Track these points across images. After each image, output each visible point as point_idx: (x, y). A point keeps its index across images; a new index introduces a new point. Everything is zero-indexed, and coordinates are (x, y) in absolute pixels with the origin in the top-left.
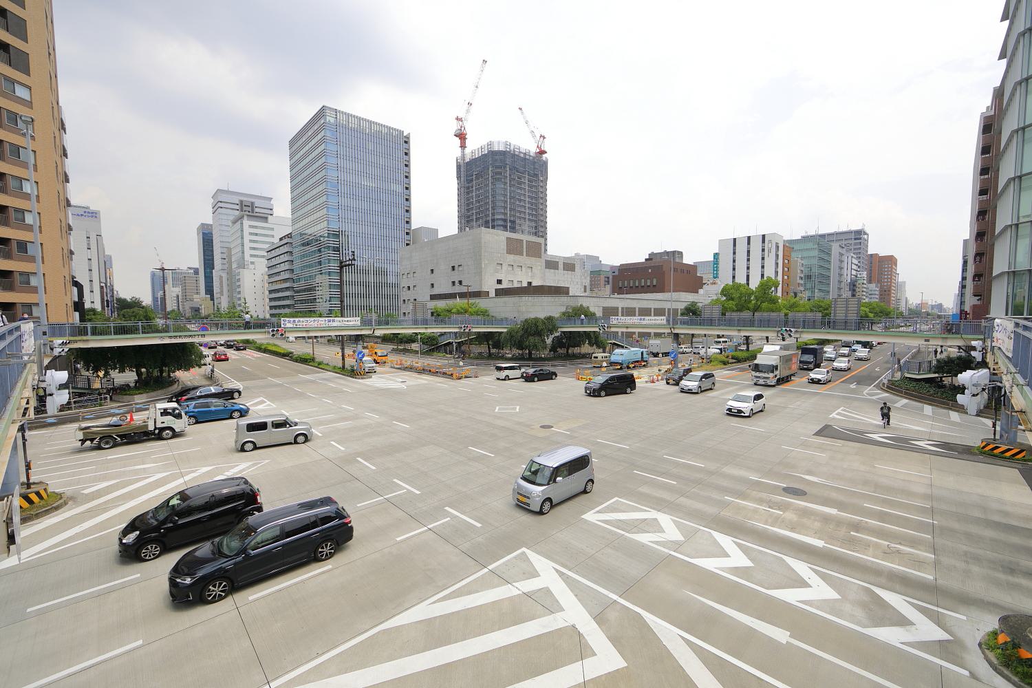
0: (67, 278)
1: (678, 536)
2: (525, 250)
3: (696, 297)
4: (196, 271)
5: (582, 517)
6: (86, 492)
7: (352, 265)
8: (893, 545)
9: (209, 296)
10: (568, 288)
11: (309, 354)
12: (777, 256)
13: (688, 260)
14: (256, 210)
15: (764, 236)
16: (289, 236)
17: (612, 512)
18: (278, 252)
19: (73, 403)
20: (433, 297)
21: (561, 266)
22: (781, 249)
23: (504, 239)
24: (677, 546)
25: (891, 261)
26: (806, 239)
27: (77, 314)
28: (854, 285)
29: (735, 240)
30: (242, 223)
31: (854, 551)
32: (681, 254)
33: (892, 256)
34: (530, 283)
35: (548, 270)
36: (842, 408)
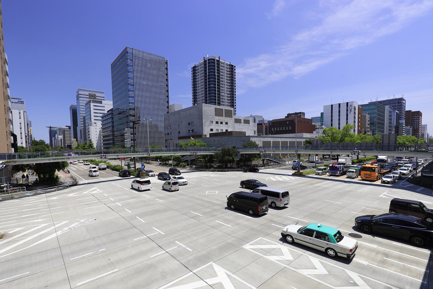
0: (8, 132)
1: (291, 258)
2: (224, 114)
3: (312, 135)
4: (70, 127)
5: (243, 247)
6: (10, 232)
7: (138, 123)
8: (406, 265)
9: (75, 139)
10: (245, 132)
11: (119, 165)
12: (355, 113)
13: (308, 116)
14: (97, 98)
15: (347, 103)
16: (111, 110)
17: (258, 244)
18: (107, 118)
19: (9, 190)
20: (180, 138)
21: (242, 121)
22: (357, 109)
23: (213, 109)
24: (289, 262)
25: (418, 114)
26: (371, 104)
27: (13, 149)
28: (398, 127)
29: (332, 105)
30: (90, 105)
31: (384, 268)
32: (304, 114)
33: (419, 111)
34: (227, 130)
35: (236, 124)
36: (387, 192)
